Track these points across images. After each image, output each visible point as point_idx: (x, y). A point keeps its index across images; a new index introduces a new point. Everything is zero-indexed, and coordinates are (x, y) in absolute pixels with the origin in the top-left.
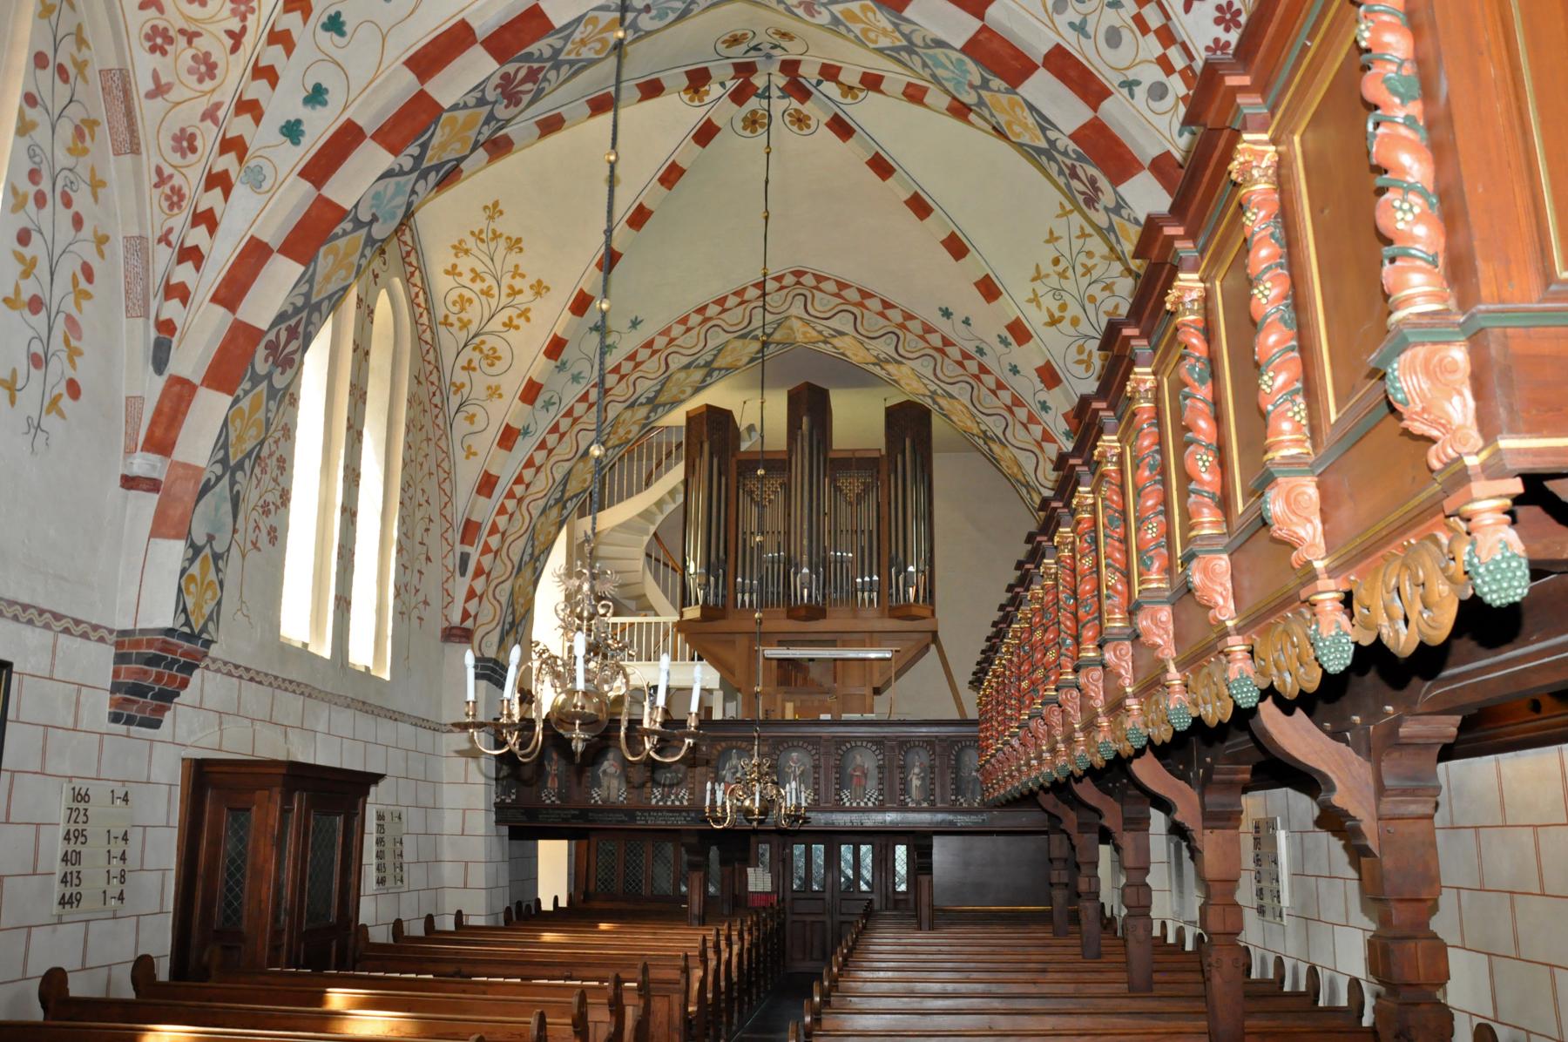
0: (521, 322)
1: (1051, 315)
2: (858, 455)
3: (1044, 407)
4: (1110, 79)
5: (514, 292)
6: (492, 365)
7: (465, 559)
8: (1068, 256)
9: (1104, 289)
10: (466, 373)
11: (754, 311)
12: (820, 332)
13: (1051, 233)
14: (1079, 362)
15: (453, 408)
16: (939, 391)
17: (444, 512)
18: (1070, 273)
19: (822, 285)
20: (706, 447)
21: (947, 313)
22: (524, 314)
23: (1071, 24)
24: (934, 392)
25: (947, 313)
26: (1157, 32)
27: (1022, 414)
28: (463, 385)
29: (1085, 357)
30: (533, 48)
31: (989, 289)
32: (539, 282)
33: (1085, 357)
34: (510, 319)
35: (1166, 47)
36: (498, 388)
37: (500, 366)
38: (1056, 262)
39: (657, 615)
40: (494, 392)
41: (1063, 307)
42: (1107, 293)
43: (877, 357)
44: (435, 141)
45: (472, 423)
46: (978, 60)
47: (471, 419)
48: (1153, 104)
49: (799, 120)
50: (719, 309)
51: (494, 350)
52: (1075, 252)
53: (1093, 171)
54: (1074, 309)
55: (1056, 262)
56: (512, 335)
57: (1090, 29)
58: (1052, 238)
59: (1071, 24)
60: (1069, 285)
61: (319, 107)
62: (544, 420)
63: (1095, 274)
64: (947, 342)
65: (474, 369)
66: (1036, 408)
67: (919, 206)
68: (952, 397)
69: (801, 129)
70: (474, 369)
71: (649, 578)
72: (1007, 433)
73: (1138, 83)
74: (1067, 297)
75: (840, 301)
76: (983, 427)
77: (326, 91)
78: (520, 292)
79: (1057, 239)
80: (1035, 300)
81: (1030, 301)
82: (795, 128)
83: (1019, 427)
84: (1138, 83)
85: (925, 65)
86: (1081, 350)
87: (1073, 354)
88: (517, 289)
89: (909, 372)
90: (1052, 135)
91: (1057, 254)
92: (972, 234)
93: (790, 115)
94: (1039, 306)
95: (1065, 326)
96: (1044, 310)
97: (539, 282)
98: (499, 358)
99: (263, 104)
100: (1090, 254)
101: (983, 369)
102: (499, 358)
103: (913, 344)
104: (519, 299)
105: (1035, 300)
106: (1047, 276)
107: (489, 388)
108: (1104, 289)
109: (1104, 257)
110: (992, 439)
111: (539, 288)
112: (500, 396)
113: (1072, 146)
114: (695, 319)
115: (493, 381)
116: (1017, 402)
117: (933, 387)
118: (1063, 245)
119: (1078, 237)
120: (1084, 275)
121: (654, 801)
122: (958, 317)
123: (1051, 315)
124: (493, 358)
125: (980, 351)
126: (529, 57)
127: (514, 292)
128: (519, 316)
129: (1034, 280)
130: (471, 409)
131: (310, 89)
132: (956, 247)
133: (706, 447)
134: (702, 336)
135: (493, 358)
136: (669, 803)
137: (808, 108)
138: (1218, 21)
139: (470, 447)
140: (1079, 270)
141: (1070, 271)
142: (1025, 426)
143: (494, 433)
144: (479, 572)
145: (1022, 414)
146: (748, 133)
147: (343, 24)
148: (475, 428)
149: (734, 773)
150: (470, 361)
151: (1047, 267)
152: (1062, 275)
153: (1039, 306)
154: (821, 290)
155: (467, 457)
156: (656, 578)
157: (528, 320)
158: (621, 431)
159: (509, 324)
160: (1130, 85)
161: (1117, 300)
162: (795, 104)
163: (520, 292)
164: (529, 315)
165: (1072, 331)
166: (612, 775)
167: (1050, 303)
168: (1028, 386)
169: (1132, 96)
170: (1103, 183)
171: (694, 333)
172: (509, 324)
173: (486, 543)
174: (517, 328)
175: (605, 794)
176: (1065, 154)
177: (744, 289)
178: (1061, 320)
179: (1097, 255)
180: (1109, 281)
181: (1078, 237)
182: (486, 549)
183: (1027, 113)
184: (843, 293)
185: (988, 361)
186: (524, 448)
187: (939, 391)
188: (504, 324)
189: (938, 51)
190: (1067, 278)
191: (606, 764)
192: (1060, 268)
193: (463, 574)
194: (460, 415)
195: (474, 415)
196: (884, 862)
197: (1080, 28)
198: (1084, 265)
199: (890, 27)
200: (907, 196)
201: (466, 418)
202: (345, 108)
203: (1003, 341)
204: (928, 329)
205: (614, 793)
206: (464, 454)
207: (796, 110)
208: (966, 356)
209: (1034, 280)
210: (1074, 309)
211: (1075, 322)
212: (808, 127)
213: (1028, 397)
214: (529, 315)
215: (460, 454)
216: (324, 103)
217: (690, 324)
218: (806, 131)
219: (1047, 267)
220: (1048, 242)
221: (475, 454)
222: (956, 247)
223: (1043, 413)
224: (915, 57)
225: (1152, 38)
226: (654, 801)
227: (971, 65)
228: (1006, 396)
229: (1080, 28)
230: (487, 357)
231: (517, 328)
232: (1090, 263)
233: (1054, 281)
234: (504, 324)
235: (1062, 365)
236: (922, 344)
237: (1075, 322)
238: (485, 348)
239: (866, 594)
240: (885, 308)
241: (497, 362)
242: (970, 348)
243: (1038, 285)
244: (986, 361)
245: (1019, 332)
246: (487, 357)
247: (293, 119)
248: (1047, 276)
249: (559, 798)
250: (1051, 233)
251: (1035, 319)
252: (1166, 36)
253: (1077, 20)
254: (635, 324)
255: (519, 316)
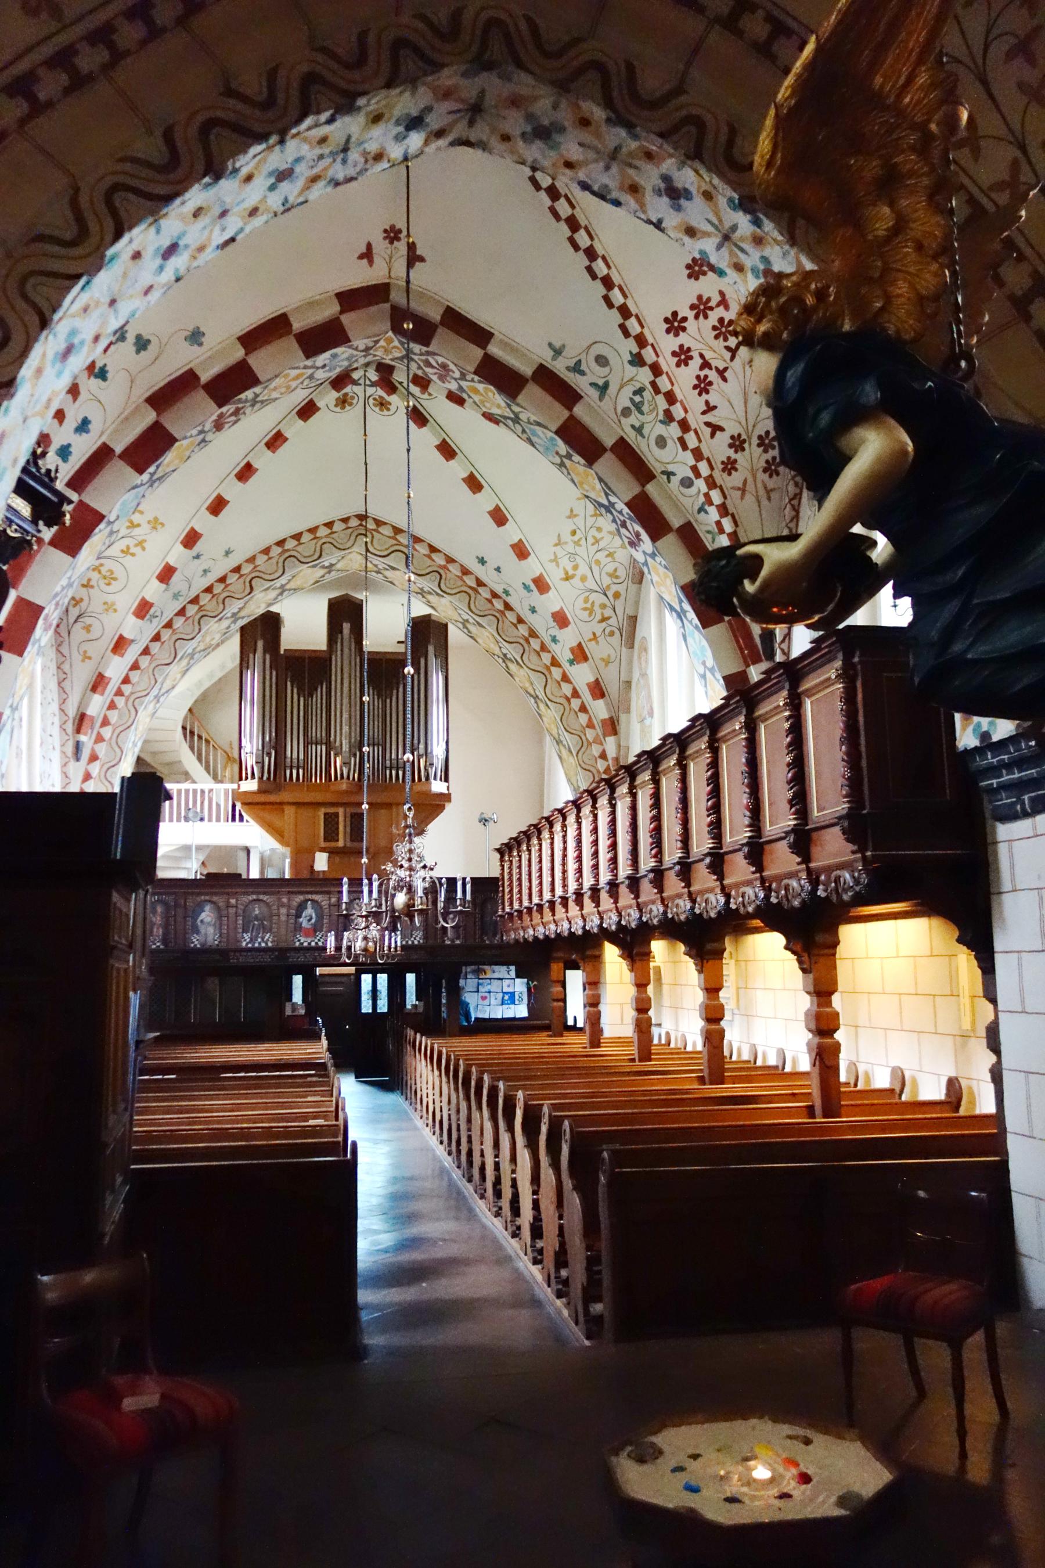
0: (137, 550)
1: (567, 573)
2: (388, 657)
3: (554, 640)
4: (657, 468)
5: (133, 525)
6: (109, 584)
7: (78, 747)
8: (583, 529)
9: (607, 556)
10: (85, 589)
11: (324, 546)
12: (376, 566)
13: (572, 511)
14: (585, 609)
15: (72, 620)
16: (471, 620)
17: (63, 707)
18: (583, 542)
19: (380, 529)
20: (260, 644)
21: (482, 561)
22: (141, 544)
23: (633, 427)
24: (467, 621)
25: (482, 561)
26: (692, 450)
27: (535, 644)
28: (82, 600)
29: (589, 605)
30: (243, 396)
31: (521, 551)
32: (156, 519)
33: (589, 605)
34: (128, 547)
35: (697, 461)
36: (113, 604)
37: (115, 586)
38: (574, 533)
39: (194, 782)
40: (109, 607)
41: (576, 567)
42: (609, 559)
43: (422, 589)
44: (166, 462)
45: (88, 631)
46: (567, 442)
47: (88, 628)
48: (681, 488)
49: (382, 404)
50: (296, 543)
51: (112, 572)
52: (589, 525)
53: (638, 528)
54: (583, 569)
55: (574, 533)
56: (128, 560)
57: (646, 431)
58: (572, 515)
59: (633, 427)
60: (581, 551)
61: (84, 434)
62: (150, 628)
63: (602, 544)
64: (480, 583)
65: (92, 587)
66: (547, 640)
67: (474, 484)
68: (482, 626)
69: (381, 410)
70: (92, 587)
71: (185, 747)
72: (442, 585)
73: (674, 474)
74: (579, 560)
75: (395, 542)
76: (504, 651)
77: (90, 422)
78: (139, 525)
79: (576, 516)
80: (555, 560)
81: (551, 561)
82: (377, 409)
83: (533, 654)
84: (674, 474)
85: (524, 431)
86: (586, 600)
87: (580, 603)
88: (135, 523)
89: (448, 604)
90: (613, 499)
91: (575, 527)
92: (512, 507)
93: (375, 399)
94: (558, 565)
95: (576, 581)
96: (561, 566)
97: (156, 519)
98: (115, 579)
99: (52, 436)
100: (599, 529)
101: (508, 606)
102: (115, 579)
103: (452, 582)
104: (137, 531)
105: (555, 560)
106: (566, 543)
107: (105, 603)
108: (607, 556)
109: (610, 533)
110: (510, 660)
111: (156, 524)
112: (115, 611)
113: (626, 510)
114: (276, 551)
115: (110, 598)
116: (533, 634)
117: (466, 617)
118: (579, 521)
119: (592, 516)
120: (593, 544)
121: (244, 944)
122: (491, 564)
123: (567, 573)
124: (110, 578)
125: (506, 592)
126: (240, 401)
127: (133, 525)
128: (136, 545)
129: (556, 545)
130: (88, 621)
131: (79, 421)
132: (499, 517)
133: (260, 644)
134: (280, 564)
135: (110, 578)
136: (256, 945)
137: (394, 399)
138: (731, 446)
139: (85, 652)
140: (590, 540)
141: (583, 542)
142: (538, 653)
143: (108, 640)
144: (94, 758)
145: (535, 644)
146: (338, 409)
147: (106, 372)
148: (90, 636)
149: (310, 920)
150: (89, 580)
151: (566, 537)
152: (577, 543)
153: (558, 565)
154: (379, 532)
155: (83, 661)
156: (192, 748)
157: (144, 549)
158: (208, 639)
159: (126, 552)
160: (669, 474)
161: (617, 565)
162: (381, 392)
163: (139, 525)
164: (144, 545)
165: (580, 585)
166: (209, 924)
167: (566, 563)
168: (543, 624)
169: (669, 482)
170: (644, 536)
171: (274, 561)
172: (126, 552)
173: (99, 733)
174: (133, 555)
175: (202, 940)
176: (621, 512)
177: (317, 528)
178: (573, 576)
179: (605, 530)
180: (611, 550)
181: (592, 516)
182: (100, 739)
183: (597, 481)
184: (398, 537)
185: (512, 601)
186: (132, 653)
187: (471, 620)
188: (122, 551)
189: (537, 428)
190: (580, 546)
191: (203, 916)
192: (576, 538)
193: (78, 759)
194: (78, 625)
195: (90, 626)
196: (397, 988)
197: (639, 430)
198: (594, 537)
199: (503, 404)
200: (465, 475)
201: (84, 628)
202: (102, 433)
203: (526, 587)
204: (466, 572)
205: (210, 939)
206: (81, 658)
207: (380, 397)
208: (495, 595)
209: (556, 545)
210: (583, 569)
211: (584, 579)
212: (388, 409)
213: (541, 632)
214: (144, 545)
215: (77, 657)
216: (87, 432)
217: (271, 554)
218: (385, 412)
219: (566, 537)
220: (569, 517)
221: (90, 658)
222: (499, 517)
223: (553, 644)
224: (517, 425)
225: (689, 453)
226: (244, 944)
227: (560, 442)
228: (523, 630)
229: (639, 430)
230: (105, 578)
231: (133, 555)
232: (599, 536)
233: (570, 548)
234: (122, 551)
235: (571, 610)
236: (460, 583)
237: (584, 579)
238: (103, 570)
239: (394, 772)
240: (562, 680)
241: (113, 582)
242: (499, 590)
243: (558, 548)
244: (509, 599)
245: (541, 585)
246: (105, 578)
247: (65, 443)
248: (566, 543)
249: (163, 944)
250: (572, 511)
251: (554, 576)
252: (698, 454)
253: (637, 425)
254: (228, 553)
255: (136, 545)
